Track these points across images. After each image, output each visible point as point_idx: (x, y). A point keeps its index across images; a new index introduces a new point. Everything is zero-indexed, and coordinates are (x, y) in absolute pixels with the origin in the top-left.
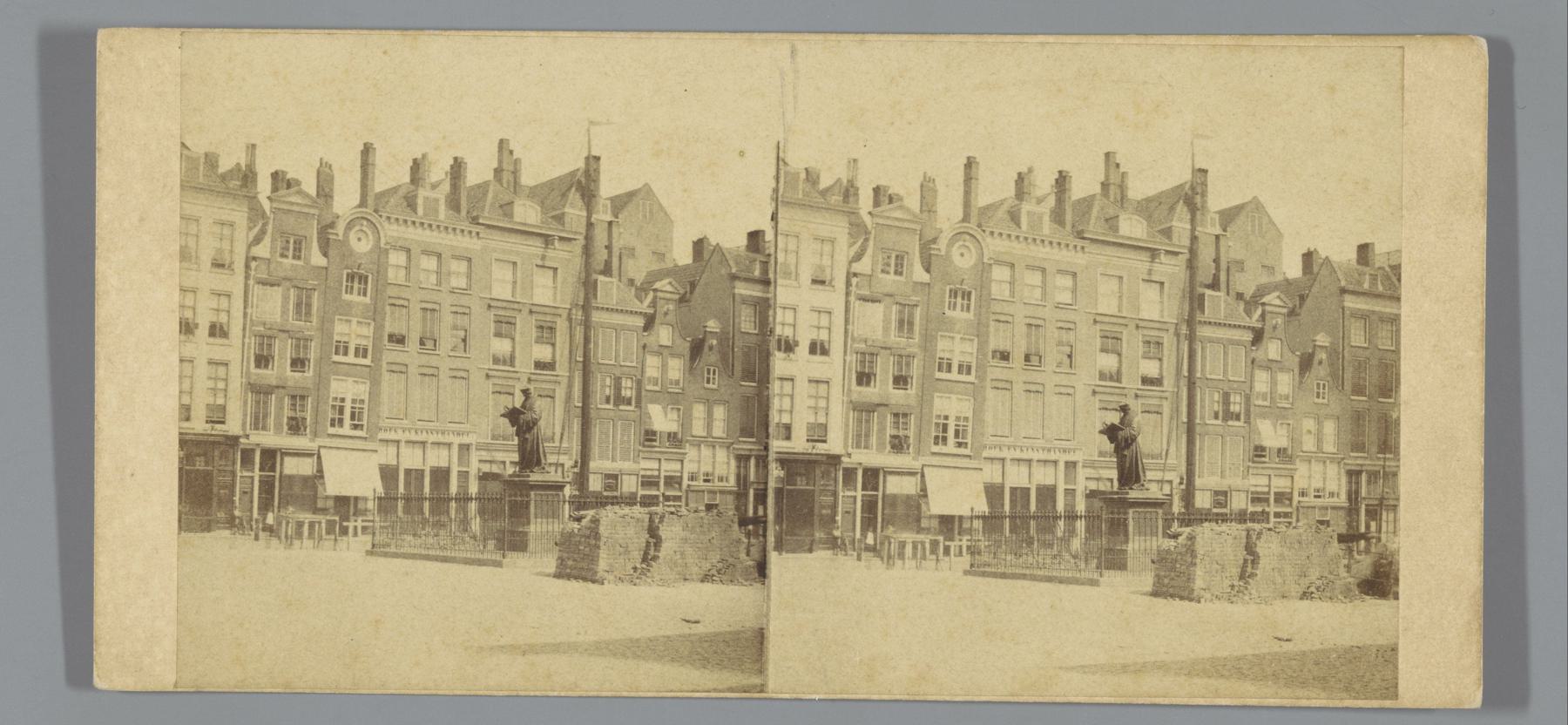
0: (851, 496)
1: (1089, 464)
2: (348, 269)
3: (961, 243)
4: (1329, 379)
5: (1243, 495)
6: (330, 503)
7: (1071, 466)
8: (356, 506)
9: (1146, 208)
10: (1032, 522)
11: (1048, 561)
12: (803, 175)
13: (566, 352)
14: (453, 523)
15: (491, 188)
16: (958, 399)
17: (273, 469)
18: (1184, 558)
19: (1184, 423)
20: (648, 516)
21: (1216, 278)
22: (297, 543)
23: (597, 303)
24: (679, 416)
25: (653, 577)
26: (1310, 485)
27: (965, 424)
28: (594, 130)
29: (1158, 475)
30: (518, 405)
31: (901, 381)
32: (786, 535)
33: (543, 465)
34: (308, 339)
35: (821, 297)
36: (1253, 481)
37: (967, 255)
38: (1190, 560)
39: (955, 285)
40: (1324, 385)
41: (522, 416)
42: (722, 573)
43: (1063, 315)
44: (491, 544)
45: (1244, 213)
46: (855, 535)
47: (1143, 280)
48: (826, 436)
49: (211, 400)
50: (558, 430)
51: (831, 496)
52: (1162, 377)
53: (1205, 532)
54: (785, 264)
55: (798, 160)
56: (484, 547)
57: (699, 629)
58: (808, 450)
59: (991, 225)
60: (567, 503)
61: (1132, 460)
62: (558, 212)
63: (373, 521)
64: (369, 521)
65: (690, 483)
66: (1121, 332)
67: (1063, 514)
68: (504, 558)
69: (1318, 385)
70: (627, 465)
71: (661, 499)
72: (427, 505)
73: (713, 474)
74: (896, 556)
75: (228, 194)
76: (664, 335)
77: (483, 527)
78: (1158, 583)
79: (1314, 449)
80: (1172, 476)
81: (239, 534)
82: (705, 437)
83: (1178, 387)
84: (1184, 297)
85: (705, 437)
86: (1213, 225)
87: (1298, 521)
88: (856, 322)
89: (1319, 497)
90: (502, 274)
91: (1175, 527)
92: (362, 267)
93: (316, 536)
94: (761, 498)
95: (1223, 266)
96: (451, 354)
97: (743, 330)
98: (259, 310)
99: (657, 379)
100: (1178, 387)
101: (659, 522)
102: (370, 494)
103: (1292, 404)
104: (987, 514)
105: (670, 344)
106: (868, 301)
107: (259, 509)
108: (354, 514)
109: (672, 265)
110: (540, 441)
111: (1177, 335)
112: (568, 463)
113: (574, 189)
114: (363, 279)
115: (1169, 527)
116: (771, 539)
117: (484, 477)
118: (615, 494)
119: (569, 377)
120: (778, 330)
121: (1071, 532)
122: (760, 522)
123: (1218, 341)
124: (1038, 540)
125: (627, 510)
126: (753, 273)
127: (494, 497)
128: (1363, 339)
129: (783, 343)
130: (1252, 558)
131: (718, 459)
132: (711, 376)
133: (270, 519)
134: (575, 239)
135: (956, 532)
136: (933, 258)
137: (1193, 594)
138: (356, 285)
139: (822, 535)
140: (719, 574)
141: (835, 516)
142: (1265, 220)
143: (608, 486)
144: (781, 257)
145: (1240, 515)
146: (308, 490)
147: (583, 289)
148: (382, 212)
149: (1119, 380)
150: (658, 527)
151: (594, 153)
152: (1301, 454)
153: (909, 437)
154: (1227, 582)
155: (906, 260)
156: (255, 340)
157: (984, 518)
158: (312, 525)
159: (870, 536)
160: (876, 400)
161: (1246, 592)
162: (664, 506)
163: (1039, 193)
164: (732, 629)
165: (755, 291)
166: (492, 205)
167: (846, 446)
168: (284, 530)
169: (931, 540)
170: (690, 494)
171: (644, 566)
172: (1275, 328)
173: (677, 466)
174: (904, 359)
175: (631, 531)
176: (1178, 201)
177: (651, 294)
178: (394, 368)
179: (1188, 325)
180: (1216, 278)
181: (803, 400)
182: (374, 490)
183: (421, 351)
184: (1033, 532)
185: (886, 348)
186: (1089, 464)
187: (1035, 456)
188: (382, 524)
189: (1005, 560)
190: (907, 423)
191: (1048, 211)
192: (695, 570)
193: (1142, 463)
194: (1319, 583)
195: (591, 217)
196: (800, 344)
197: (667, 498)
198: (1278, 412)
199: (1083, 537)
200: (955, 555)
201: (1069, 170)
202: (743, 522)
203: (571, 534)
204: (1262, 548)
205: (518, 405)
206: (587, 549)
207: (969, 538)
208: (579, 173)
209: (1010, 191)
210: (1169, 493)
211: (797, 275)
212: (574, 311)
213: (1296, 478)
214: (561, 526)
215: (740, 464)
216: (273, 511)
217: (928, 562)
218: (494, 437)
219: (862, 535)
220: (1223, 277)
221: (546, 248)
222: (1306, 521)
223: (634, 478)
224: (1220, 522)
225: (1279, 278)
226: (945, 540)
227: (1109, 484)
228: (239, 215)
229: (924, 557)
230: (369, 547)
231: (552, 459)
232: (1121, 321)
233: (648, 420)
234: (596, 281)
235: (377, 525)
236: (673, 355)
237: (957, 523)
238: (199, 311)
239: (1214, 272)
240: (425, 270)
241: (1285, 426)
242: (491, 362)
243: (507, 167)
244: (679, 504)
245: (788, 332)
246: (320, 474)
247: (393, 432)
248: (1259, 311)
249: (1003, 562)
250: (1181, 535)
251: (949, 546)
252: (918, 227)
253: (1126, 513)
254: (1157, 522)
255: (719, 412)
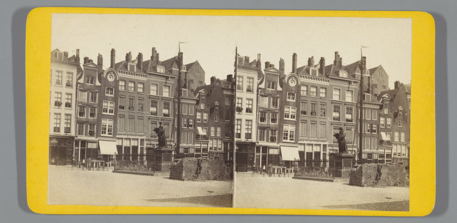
0: (258, 155)
1: (330, 145)
2: (107, 86)
3: (291, 79)
4: (403, 120)
5: (377, 155)
6: (102, 157)
7: (325, 146)
8: (109, 158)
9: (164, 64)
10: (313, 163)
11: (318, 174)
12: (244, 59)
13: (173, 112)
14: (139, 163)
15: (150, 62)
16: (109, 120)
17: (85, 147)
18: (179, 168)
19: (359, 133)
20: (377, 166)
21: (369, 89)
22: (92, 169)
23: (365, 101)
24: (207, 131)
25: (199, 179)
26: (397, 152)
27: (293, 133)
28: (181, 44)
29: (351, 149)
30: (158, 127)
31: (92, 115)
32: (239, 167)
33: (346, 151)
34: (276, 113)
35: (249, 95)
36: (380, 151)
37: (112, 78)
38: (360, 174)
39: (108, 87)
40: (401, 122)
41: (160, 131)
42: (220, 177)
43: (322, 101)
44: (150, 169)
45: (377, 70)
46: (260, 167)
47: (347, 90)
48: (70, 131)
49: (247, 132)
50: (170, 135)
51: (253, 155)
52: (169, 114)
53: (365, 165)
54: (239, 85)
55: (242, 54)
56: (148, 170)
57: (390, 201)
58: (245, 141)
59: (301, 73)
60: (173, 157)
61: (343, 144)
62: (170, 69)
63: (115, 162)
64: (114, 162)
65: (210, 150)
66: (157, 101)
67: (322, 160)
68: (154, 173)
69: (399, 122)
70: (375, 151)
71: (201, 155)
72: (131, 157)
73: (401, 153)
74: (272, 173)
75: (72, 64)
76: (202, 106)
77: (148, 165)
78: (351, 181)
79: (398, 141)
80: (355, 149)
81: (256, 172)
82: (214, 137)
83: (357, 122)
84: (359, 95)
85: (214, 137)
86: (368, 74)
87: (393, 163)
88: (79, 97)
89: (400, 155)
90: (153, 88)
91: (356, 164)
92: (111, 86)
93: (98, 167)
94: (231, 155)
95: (187, 81)
96: (320, 117)
97: (226, 105)
98: (261, 104)
99: (200, 119)
100: (357, 122)
101: (201, 162)
102: (114, 154)
103: (208, 122)
104: (299, 160)
105: (204, 109)
106: (83, 91)
107: (80, 159)
108: (109, 160)
109: (204, 85)
110: (345, 144)
111: (357, 107)
112: (173, 145)
113: (175, 62)
114: (293, 95)
115: (355, 164)
116: (235, 168)
117: (148, 149)
118: (187, 154)
119: (174, 119)
120: (237, 105)
121: (325, 165)
122: (231, 162)
123: (369, 108)
124: (315, 168)
125: (191, 159)
126: (229, 87)
127: (319, 160)
128: (229, 103)
129: (238, 109)
130: (379, 174)
131: (218, 143)
132: (216, 118)
133: (84, 161)
134: (175, 77)
135: (290, 166)
136: (283, 83)
137: (361, 184)
138: (109, 91)
139: (250, 167)
140: (219, 177)
141: (254, 161)
142: (383, 72)
143: (185, 152)
144: (237, 83)
145: (376, 161)
146: (95, 153)
147: (178, 92)
148: (117, 69)
149: (339, 120)
150: (380, 170)
151: (181, 52)
152: (394, 143)
153: (276, 137)
154: (372, 181)
155: (275, 84)
156: (79, 108)
157: (298, 161)
158: (96, 163)
159: (264, 167)
160: (266, 126)
161: (377, 184)
162: (202, 157)
163: (315, 64)
164: (223, 194)
165: (229, 93)
166: (150, 67)
167: (76, 134)
168: (88, 165)
169: (282, 168)
170: (210, 154)
171: (196, 175)
172: (203, 100)
173: (390, 151)
174: (274, 114)
175: (372, 171)
176: (357, 67)
177: (198, 94)
178: (121, 116)
179: (360, 104)
180: (369, 89)
181: (244, 126)
182: (115, 153)
183: (129, 111)
184: (313, 166)
185: (88, 105)
186: (330, 145)
187: (314, 143)
188: (117, 163)
189: (305, 174)
190: (275, 133)
191: (136, 65)
192: (392, 182)
193: (346, 145)
194: (399, 181)
195: (180, 71)
196: (63, 104)
197: (203, 155)
198: (387, 130)
199: (328, 167)
200: (290, 173)
201: (324, 57)
202: (226, 162)
203: (175, 166)
204: (383, 171)
205: (158, 127)
206: (179, 170)
207: (294, 167)
208: (177, 58)
209: (306, 63)
210: (354, 154)
211: (62, 83)
212: (175, 99)
213: (393, 150)
214: (171, 164)
215: (225, 145)
216: (85, 159)
217: (282, 174)
218: (151, 137)
219: (262, 166)
220: (371, 89)
221: (167, 80)
222: (396, 163)
223: (377, 155)
224: (370, 163)
225: (204, 85)
226: (287, 168)
227: (336, 151)
228: (75, 71)
229: (280, 173)
230: (113, 170)
231: (168, 143)
232: (339, 102)
233: (381, 137)
234: (182, 90)
235: (116, 163)
236: (205, 112)
237: (290, 163)
238: (62, 99)
239: (368, 88)
240: (130, 87)
241: (205, 129)
242: (150, 114)
243: (338, 60)
244: (207, 157)
245: (240, 105)
246: (280, 154)
247: (303, 141)
248: (382, 99)
249: (304, 175)
250: (358, 167)
251: (288, 170)
252: (279, 74)
253: (341, 160)
254: (351, 163)
255: (219, 129)
